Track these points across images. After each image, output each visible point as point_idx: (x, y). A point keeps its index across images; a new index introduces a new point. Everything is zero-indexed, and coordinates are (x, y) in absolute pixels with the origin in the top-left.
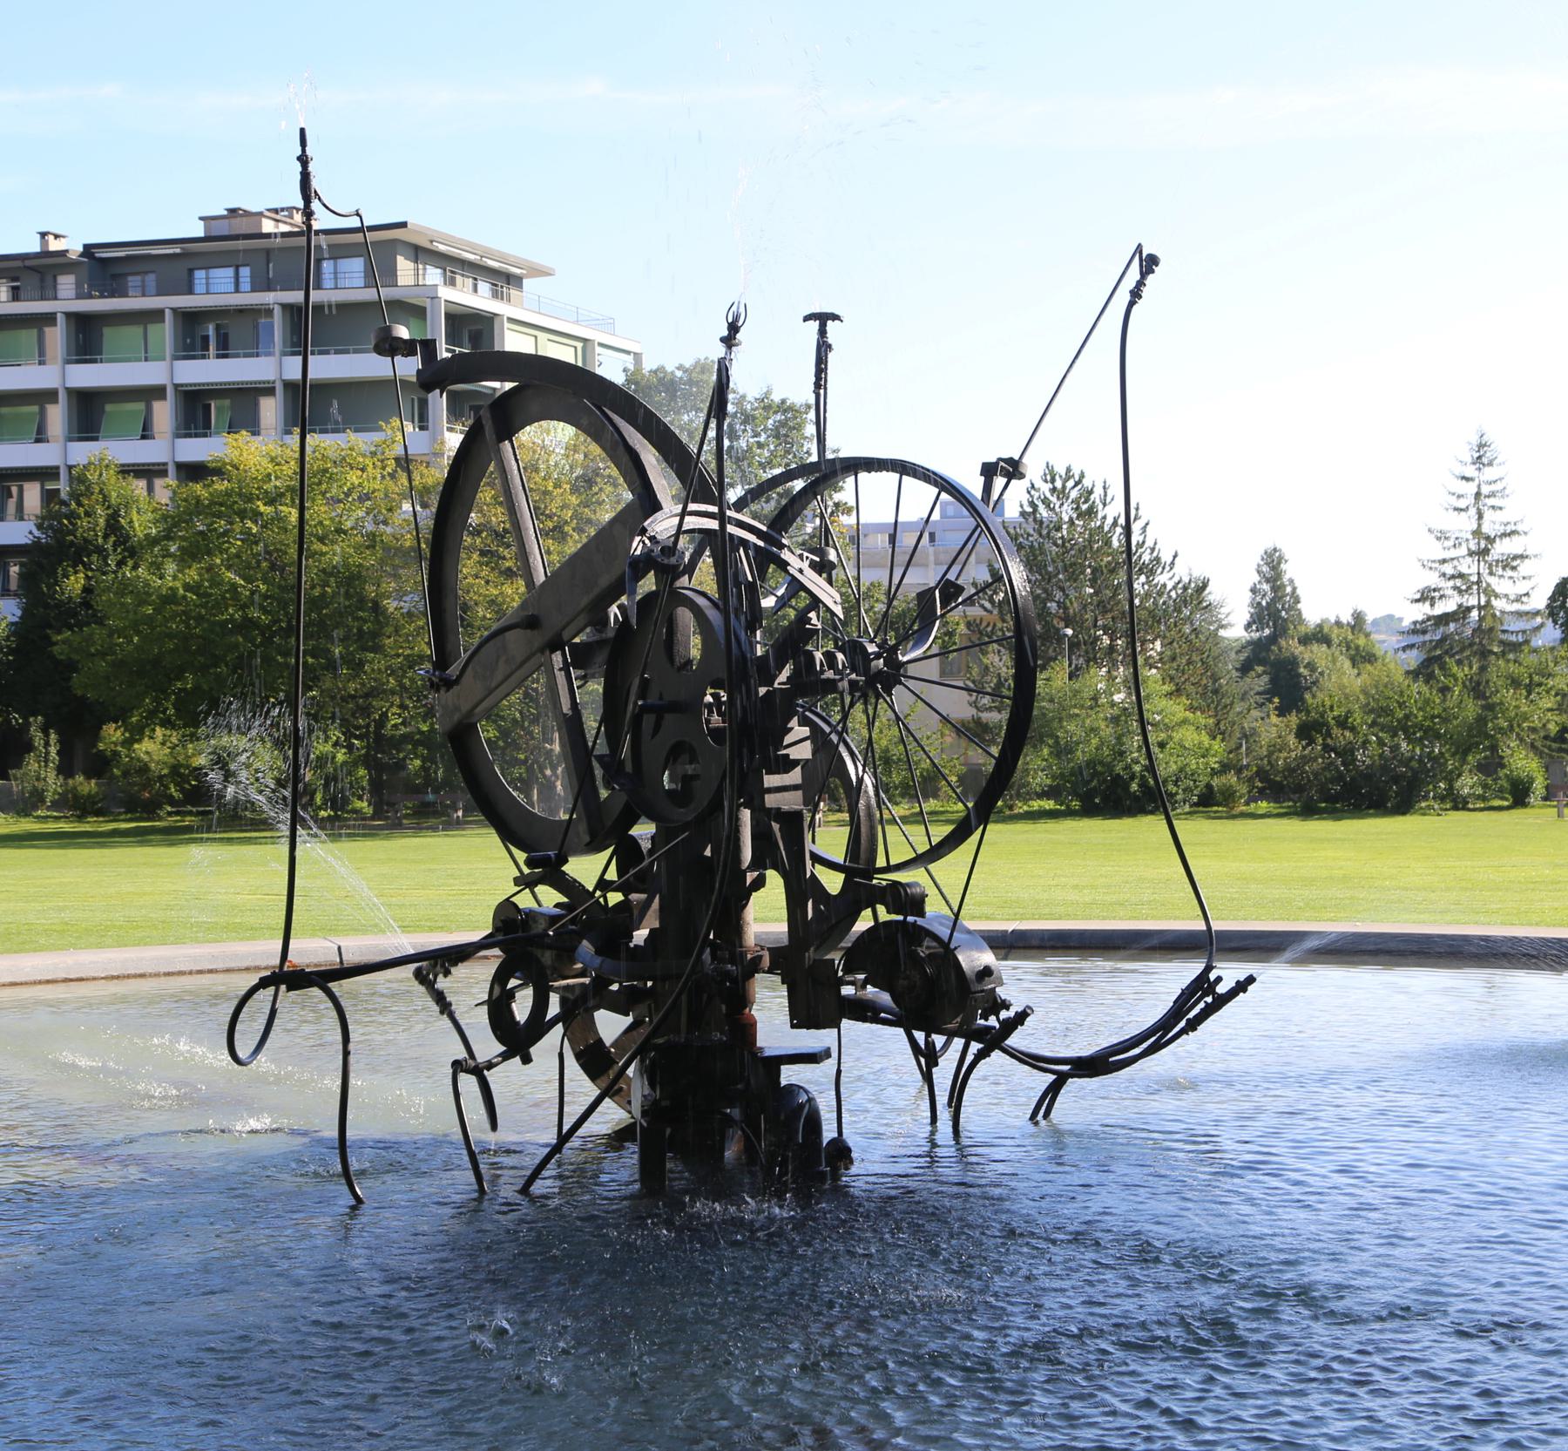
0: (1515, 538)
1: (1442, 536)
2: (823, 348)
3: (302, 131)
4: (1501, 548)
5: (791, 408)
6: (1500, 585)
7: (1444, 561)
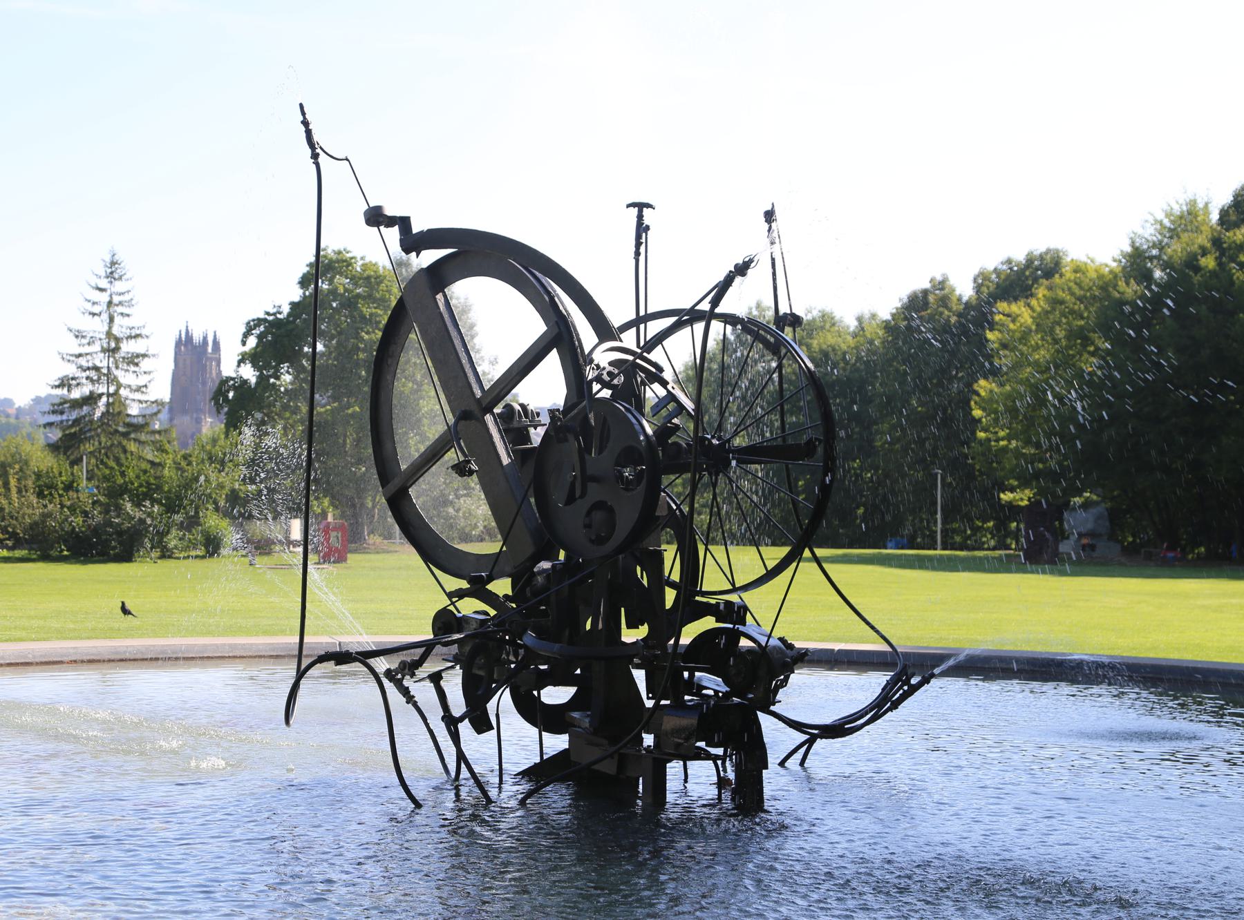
0: (139, 340)
1: (79, 335)
2: (642, 229)
3: (301, 106)
4: (128, 347)
6: (126, 377)
7: (80, 355)
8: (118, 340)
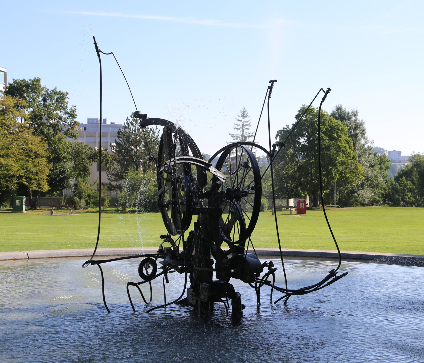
1: (233, 136)
5: (62, 94)
8: (246, 137)
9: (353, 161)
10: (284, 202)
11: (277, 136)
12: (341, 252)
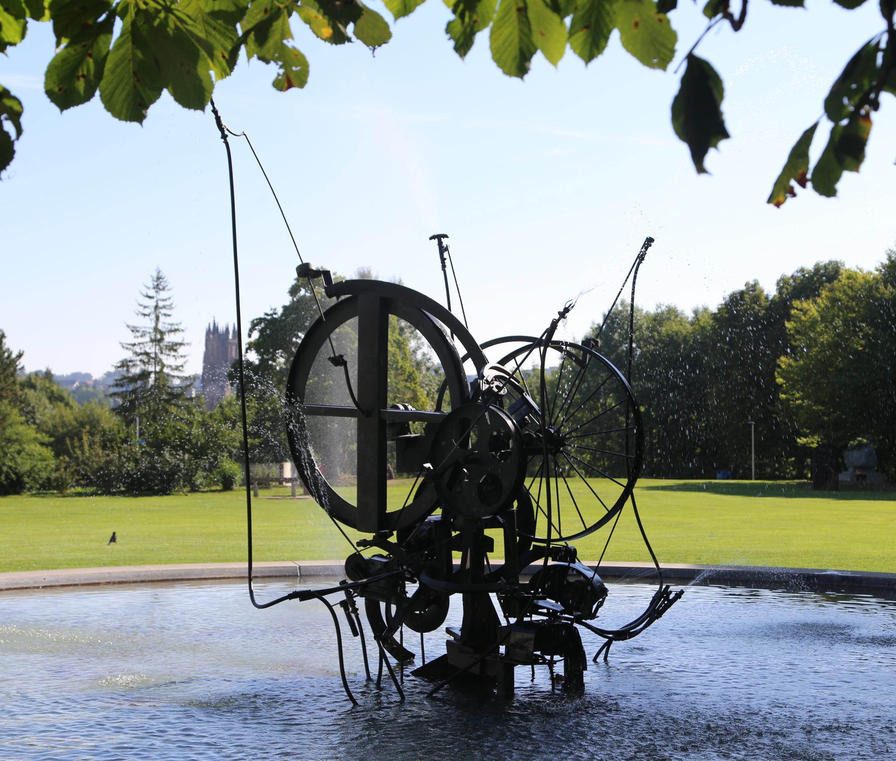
0: (178, 333)
1: (134, 330)
4: (169, 338)
7: (134, 345)
8: (162, 333)
9: (408, 384)
10: (274, 470)
11: (251, 330)
12: (661, 565)
